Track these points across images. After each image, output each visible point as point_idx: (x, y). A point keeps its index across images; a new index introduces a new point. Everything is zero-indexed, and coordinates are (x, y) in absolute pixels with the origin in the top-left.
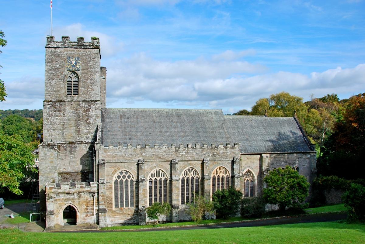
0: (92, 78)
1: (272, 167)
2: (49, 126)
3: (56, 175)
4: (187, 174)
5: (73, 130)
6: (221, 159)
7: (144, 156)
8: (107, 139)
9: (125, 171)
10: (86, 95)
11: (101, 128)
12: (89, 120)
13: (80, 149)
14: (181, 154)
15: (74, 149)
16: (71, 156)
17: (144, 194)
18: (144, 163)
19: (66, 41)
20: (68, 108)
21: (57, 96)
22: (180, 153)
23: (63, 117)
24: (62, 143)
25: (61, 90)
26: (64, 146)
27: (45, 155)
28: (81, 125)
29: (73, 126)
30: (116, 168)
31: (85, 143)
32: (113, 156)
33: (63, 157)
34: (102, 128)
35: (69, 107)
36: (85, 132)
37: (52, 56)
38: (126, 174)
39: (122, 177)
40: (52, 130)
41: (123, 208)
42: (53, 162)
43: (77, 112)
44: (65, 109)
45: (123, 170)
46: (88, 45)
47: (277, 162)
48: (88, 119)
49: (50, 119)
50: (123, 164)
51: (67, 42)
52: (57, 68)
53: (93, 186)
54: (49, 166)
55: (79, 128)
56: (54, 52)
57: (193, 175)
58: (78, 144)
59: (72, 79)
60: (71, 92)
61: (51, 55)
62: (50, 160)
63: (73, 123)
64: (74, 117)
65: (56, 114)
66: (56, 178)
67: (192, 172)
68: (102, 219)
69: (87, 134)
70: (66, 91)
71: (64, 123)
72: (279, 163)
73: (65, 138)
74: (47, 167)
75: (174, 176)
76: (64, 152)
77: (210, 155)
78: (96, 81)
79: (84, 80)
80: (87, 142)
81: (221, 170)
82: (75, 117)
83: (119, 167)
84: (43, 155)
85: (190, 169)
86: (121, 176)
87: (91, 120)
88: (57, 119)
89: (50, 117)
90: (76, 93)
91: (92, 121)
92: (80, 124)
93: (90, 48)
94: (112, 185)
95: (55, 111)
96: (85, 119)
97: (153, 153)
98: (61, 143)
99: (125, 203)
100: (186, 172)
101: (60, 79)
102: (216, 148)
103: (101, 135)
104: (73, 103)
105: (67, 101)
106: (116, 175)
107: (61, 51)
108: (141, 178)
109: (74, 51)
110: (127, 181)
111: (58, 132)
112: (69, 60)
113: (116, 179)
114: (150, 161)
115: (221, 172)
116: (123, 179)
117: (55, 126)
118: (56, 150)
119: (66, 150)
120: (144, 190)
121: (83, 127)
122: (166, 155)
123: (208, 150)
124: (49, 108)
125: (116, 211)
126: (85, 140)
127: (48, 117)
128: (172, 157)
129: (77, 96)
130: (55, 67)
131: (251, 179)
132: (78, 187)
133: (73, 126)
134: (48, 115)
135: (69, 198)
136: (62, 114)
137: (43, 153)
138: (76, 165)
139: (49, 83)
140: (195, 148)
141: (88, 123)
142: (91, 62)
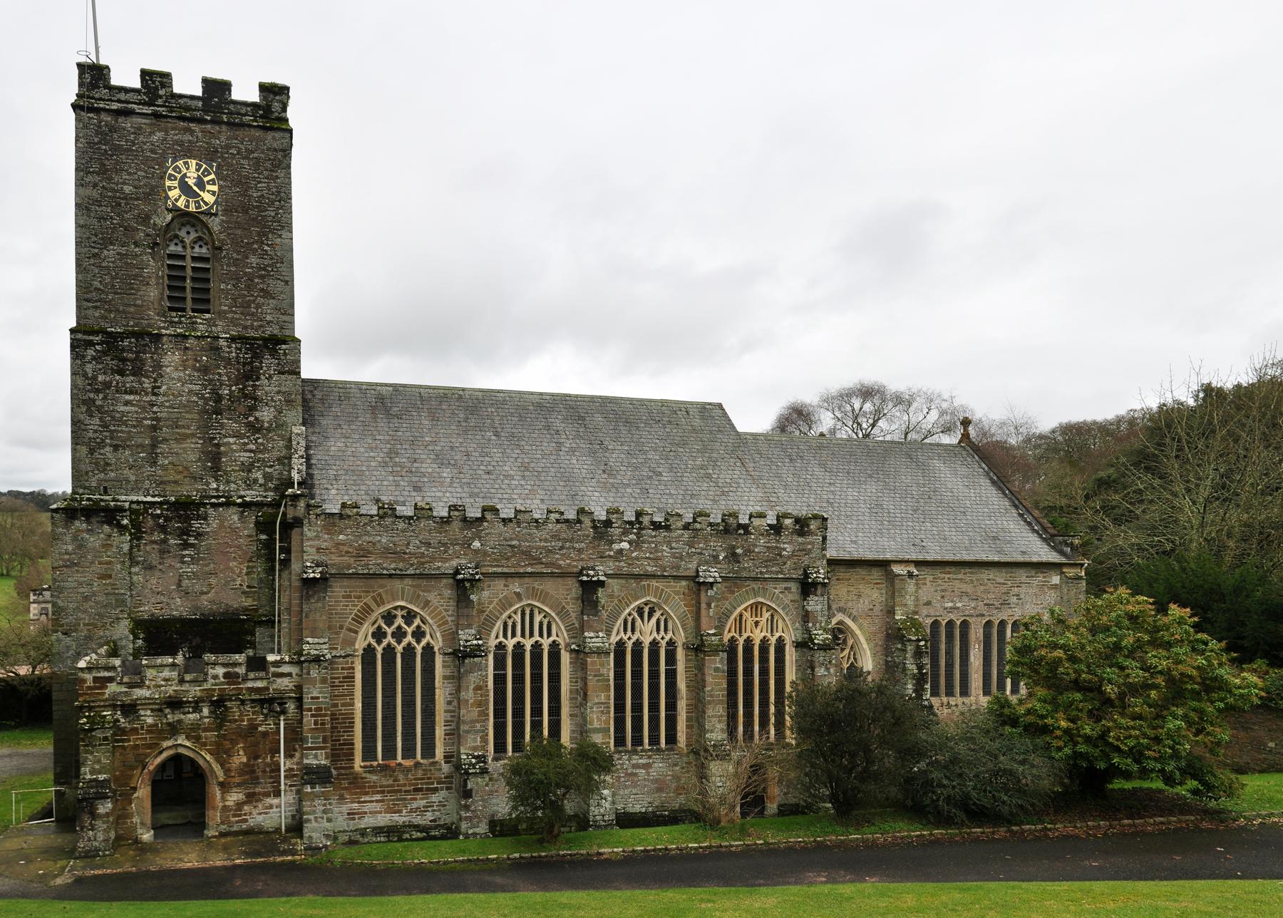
0: (266, 248)
1: (927, 616)
2: (96, 431)
3: (122, 629)
4: (633, 631)
5: (190, 452)
6: (761, 573)
7: (477, 551)
8: (330, 487)
9: (404, 612)
10: (242, 314)
11: (303, 443)
12: (258, 414)
13: (221, 526)
14: (616, 547)
15: (196, 524)
16: (184, 553)
17: (479, 704)
18: (479, 580)
19: (156, 89)
20: (171, 359)
21: (130, 313)
22: (612, 542)
23: (154, 398)
24: (149, 499)
25: (144, 288)
26: (159, 512)
27: (80, 547)
28: (223, 432)
29: (193, 435)
30: (368, 600)
31: (239, 505)
32: (360, 548)
33: (154, 558)
34: (308, 448)
35: (177, 357)
36: (241, 459)
37: (104, 147)
38: (409, 624)
39: (393, 635)
40: (108, 449)
41: (392, 763)
42: (110, 576)
43: (210, 381)
44: (158, 366)
45: (395, 608)
46: (245, 115)
47: (943, 597)
48: (252, 409)
49: (99, 403)
50: (397, 584)
51: (162, 92)
52: (125, 198)
53: (280, 670)
54: (94, 594)
55: (218, 445)
56: (112, 129)
57: (655, 634)
58: (213, 505)
59: (184, 247)
60: (184, 299)
61: (99, 143)
62: (97, 568)
63: (191, 421)
64: (195, 398)
65: (124, 383)
66: (124, 643)
67: (654, 620)
68: (314, 812)
69: (248, 468)
70: (162, 294)
71: (158, 419)
72: (952, 601)
73: (162, 483)
74: (86, 599)
75: (592, 634)
76: (157, 536)
77: (721, 558)
78: (282, 263)
79: (235, 255)
80: (247, 499)
81: (756, 616)
82: (203, 397)
83: (379, 595)
84: (70, 548)
85: (646, 610)
86: (389, 631)
87: (266, 415)
88: (127, 403)
89: (101, 396)
90: (203, 303)
91: (267, 419)
92: (222, 425)
93: (255, 124)
94: (353, 668)
95: (121, 373)
96: (242, 409)
97: (511, 539)
98: (145, 499)
99: (403, 740)
100: (630, 619)
101: (136, 245)
102: (741, 531)
103: (304, 468)
104: (190, 343)
105: (168, 332)
106: (367, 629)
107: (140, 128)
108: (467, 641)
109: (192, 132)
110: (409, 650)
111: (132, 455)
112: (174, 170)
113: (369, 645)
114: (499, 570)
115: (757, 623)
116: (393, 642)
117: (122, 431)
118: (125, 527)
119: (163, 529)
120: (478, 688)
121: (231, 440)
122: (562, 548)
123: (711, 535)
124: (94, 358)
125: (368, 775)
126: (242, 493)
127: (92, 395)
128: (582, 560)
129: (207, 316)
130: (117, 191)
131: (849, 658)
132: (215, 677)
133: (193, 435)
134: (89, 384)
135: (180, 721)
136: (147, 384)
137: (68, 538)
138: (205, 590)
139: (95, 255)
140: (667, 528)
141: (250, 426)
142: (260, 182)
